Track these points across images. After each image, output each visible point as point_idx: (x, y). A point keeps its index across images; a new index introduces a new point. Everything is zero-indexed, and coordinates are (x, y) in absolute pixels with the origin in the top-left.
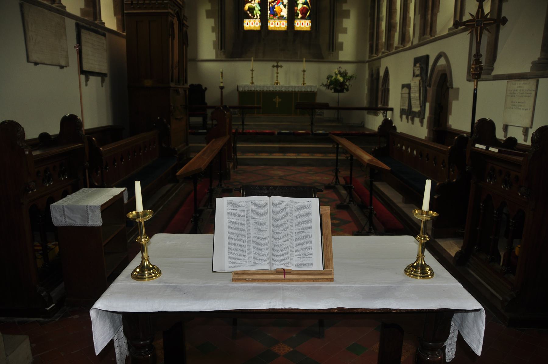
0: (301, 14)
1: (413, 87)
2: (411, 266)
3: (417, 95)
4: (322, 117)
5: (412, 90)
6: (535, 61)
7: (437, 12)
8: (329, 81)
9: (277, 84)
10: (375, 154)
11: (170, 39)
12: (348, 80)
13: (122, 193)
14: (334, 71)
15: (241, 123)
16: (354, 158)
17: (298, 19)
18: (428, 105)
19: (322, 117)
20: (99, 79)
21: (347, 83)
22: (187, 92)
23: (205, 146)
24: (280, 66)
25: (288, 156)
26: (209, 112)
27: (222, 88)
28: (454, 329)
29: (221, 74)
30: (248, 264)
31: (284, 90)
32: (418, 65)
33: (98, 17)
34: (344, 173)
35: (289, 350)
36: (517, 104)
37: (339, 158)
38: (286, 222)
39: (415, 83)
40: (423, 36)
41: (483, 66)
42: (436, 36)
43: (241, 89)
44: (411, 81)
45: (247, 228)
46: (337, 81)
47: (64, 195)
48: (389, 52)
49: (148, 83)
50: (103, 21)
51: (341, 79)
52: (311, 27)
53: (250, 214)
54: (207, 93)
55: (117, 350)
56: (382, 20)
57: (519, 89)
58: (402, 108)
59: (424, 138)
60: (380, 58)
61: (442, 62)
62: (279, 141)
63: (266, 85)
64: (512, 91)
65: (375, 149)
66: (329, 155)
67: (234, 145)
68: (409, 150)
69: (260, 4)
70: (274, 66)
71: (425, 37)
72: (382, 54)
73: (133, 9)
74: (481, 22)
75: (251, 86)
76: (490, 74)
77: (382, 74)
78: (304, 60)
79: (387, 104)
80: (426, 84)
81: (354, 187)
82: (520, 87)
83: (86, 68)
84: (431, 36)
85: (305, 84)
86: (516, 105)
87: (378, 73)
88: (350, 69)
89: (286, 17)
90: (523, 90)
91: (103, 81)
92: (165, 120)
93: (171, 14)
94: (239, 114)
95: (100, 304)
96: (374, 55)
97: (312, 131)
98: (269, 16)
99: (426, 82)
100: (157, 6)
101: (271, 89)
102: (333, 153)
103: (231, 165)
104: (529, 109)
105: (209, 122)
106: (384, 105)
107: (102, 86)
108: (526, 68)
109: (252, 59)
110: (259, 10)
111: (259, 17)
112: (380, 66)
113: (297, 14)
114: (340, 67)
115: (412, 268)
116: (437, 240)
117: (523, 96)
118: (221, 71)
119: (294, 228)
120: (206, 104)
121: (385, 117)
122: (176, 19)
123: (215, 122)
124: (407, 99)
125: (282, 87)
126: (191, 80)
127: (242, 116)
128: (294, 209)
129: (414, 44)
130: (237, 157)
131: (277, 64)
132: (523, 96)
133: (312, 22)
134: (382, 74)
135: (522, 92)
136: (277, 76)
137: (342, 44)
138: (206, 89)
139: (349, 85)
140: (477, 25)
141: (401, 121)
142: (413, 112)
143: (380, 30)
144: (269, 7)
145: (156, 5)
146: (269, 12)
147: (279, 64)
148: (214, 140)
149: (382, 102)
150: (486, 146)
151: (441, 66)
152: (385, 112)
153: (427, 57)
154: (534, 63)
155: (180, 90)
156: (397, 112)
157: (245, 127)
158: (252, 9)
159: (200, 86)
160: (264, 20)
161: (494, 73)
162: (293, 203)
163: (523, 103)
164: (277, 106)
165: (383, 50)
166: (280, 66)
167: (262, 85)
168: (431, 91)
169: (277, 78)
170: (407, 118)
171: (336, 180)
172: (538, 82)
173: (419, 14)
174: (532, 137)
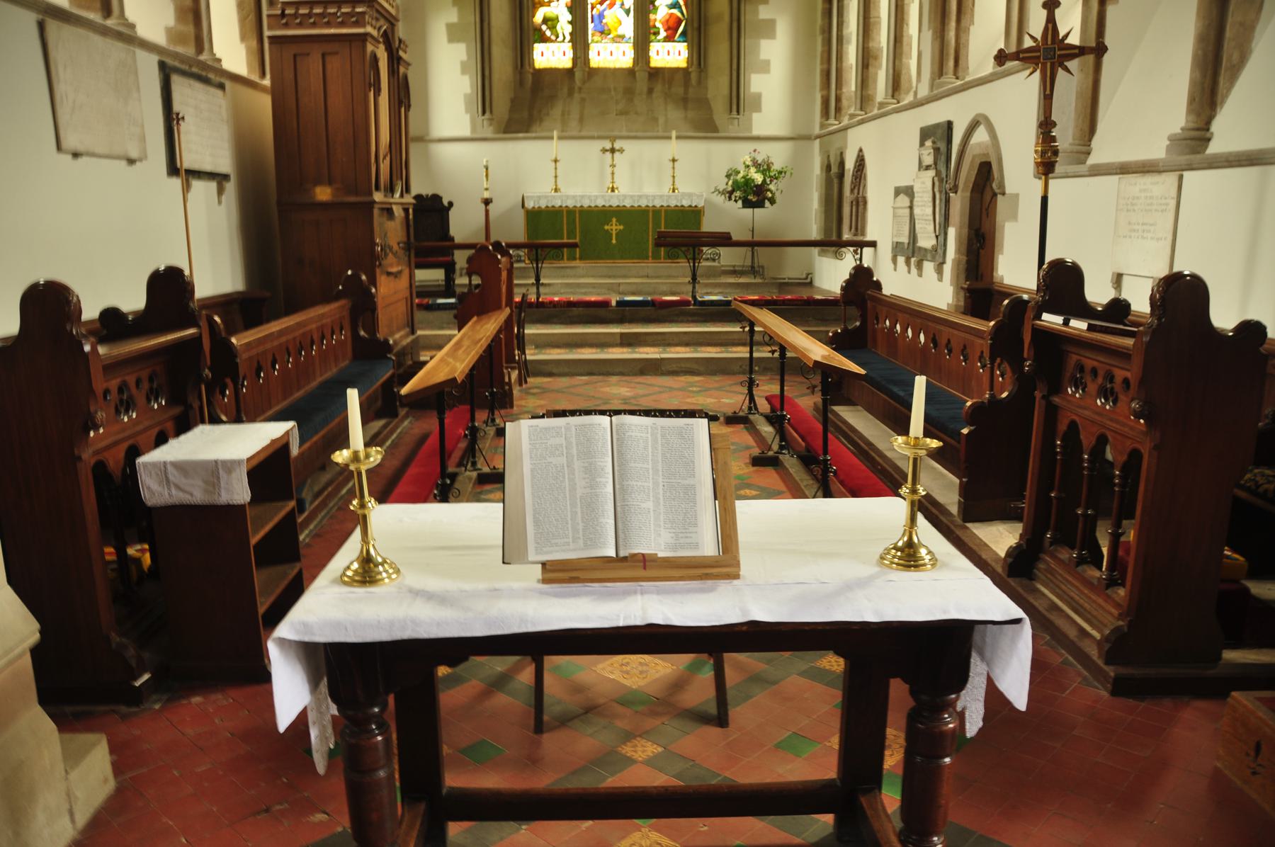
0: (666, 31)
1: (917, 192)
2: (892, 548)
3: (929, 210)
4: (716, 264)
5: (915, 199)
6: (1176, 135)
7: (970, 25)
8: (730, 183)
9: (613, 190)
10: (837, 343)
11: (372, 94)
12: (773, 178)
13: (287, 433)
14: (742, 160)
15: (533, 281)
16: (789, 354)
17: (659, 41)
18: (952, 232)
19: (716, 264)
20: (213, 185)
21: (772, 187)
22: (411, 211)
23: (455, 335)
24: (618, 150)
25: (640, 353)
26: (461, 258)
27: (487, 202)
28: (978, 670)
29: (485, 170)
30: (572, 546)
31: (628, 206)
32: (929, 143)
33: (206, 46)
34: (767, 387)
35: (655, 751)
37: (756, 355)
38: (645, 466)
39: (923, 183)
40: (939, 79)
41: (1059, 148)
42: (968, 79)
43: (530, 205)
44: (914, 180)
45: (569, 478)
46: (748, 182)
47: (161, 440)
48: (866, 114)
49: (323, 194)
50: (218, 56)
51: (758, 178)
52: (690, 60)
53: (574, 451)
54: (453, 214)
55: (314, 733)
56: (849, 42)
58: (896, 240)
59: (945, 308)
60: (846, 129)
61: (981, 136)
62: (621, 321)
63: (588, 194)
65: (835, 333)
66: (734, 349)
67: (518, 330)
68: (898, 327)
69: (571, 9)
70: (604, 151)
71: (942, 80)
72: (850, 119)
73: (286, 26)
74: (1052, 53)
75: (554, 197)
76: (1084, 162)
77: (850, 165)
78: (674, 134)
79: (863, 234)
80: (947, 186)
81: (789, 416)
82: (1145, 190)
83: (188, 159)
84: (957, 78)
85: (677, 189)
86: (1138, 230)
87: (842, 164)
88: (778, 155)
89: (630, 38)
90: (1151, 197)
91: (220, 191)
92: (364, 277)
93: (372, 37)
94: (527, 262)
95: (286, 629)
96: (832, 121)
97: (694, 297)
98: (593, 35)
99: (947, 181)
100: (340, 20)
101: (600, 203)
102: (744, 345)
103: (514, 375)
104: (1165, 239)
105: (461, 281)
106: (855, 235)
107: (220, 202)
108: (1157, 150)
109: (555, 134)
110: (570, 22)
111: (568, 37)
112: (846, 147)
113: (656, 30)
114: (755, 151)
115: (894, 551)
116: (969, 525)
117: (1151, 210)
118: (485, 163)
119: (661, 477)
120: (452, 239)
121: (858, 262)
122: (382, 47)
123: (476, 280)
125: (625, 196)
126: (420, 186)
127: (535, 265)
128: (659, 439)
129: (919, 96)
130: (526, 357)
131: (613, 145)
132: (1151, 210)
133: (690, 48)
134: (850, 165)
136: (613, 174)
137: (758, 97)
138: (451, 204)
139: (777, 190)
140: (1044, 59)
142: (920, 248)
143: (844, 64)
144: (592, 15)
145: (338, 17)
146: (591, 26)
147: (617, 145)
148: (475, 318)
149: (850, 230)
150: (1063, 318)
151: (979, 144)
152: (859, 251)
153: (949, 125)
154: (1173, 139)
155: (394, 207)
156: (885, 249)
157: (542, 290)
158: (550, 21)
159: (436, 198)
160: (580, 41)
161: (1092, 160)
162: (656, 428)
163: (1151, 225)
164: (614, 241)
165: (852, 111)
166: (618, 150)
167: (578, 194)
168: (959, 203)
169: (613, 179)
170: (908, 263)
171: (750, 403)
172: (1181, 178)
173: (929, 29)
174: (1151, 295)
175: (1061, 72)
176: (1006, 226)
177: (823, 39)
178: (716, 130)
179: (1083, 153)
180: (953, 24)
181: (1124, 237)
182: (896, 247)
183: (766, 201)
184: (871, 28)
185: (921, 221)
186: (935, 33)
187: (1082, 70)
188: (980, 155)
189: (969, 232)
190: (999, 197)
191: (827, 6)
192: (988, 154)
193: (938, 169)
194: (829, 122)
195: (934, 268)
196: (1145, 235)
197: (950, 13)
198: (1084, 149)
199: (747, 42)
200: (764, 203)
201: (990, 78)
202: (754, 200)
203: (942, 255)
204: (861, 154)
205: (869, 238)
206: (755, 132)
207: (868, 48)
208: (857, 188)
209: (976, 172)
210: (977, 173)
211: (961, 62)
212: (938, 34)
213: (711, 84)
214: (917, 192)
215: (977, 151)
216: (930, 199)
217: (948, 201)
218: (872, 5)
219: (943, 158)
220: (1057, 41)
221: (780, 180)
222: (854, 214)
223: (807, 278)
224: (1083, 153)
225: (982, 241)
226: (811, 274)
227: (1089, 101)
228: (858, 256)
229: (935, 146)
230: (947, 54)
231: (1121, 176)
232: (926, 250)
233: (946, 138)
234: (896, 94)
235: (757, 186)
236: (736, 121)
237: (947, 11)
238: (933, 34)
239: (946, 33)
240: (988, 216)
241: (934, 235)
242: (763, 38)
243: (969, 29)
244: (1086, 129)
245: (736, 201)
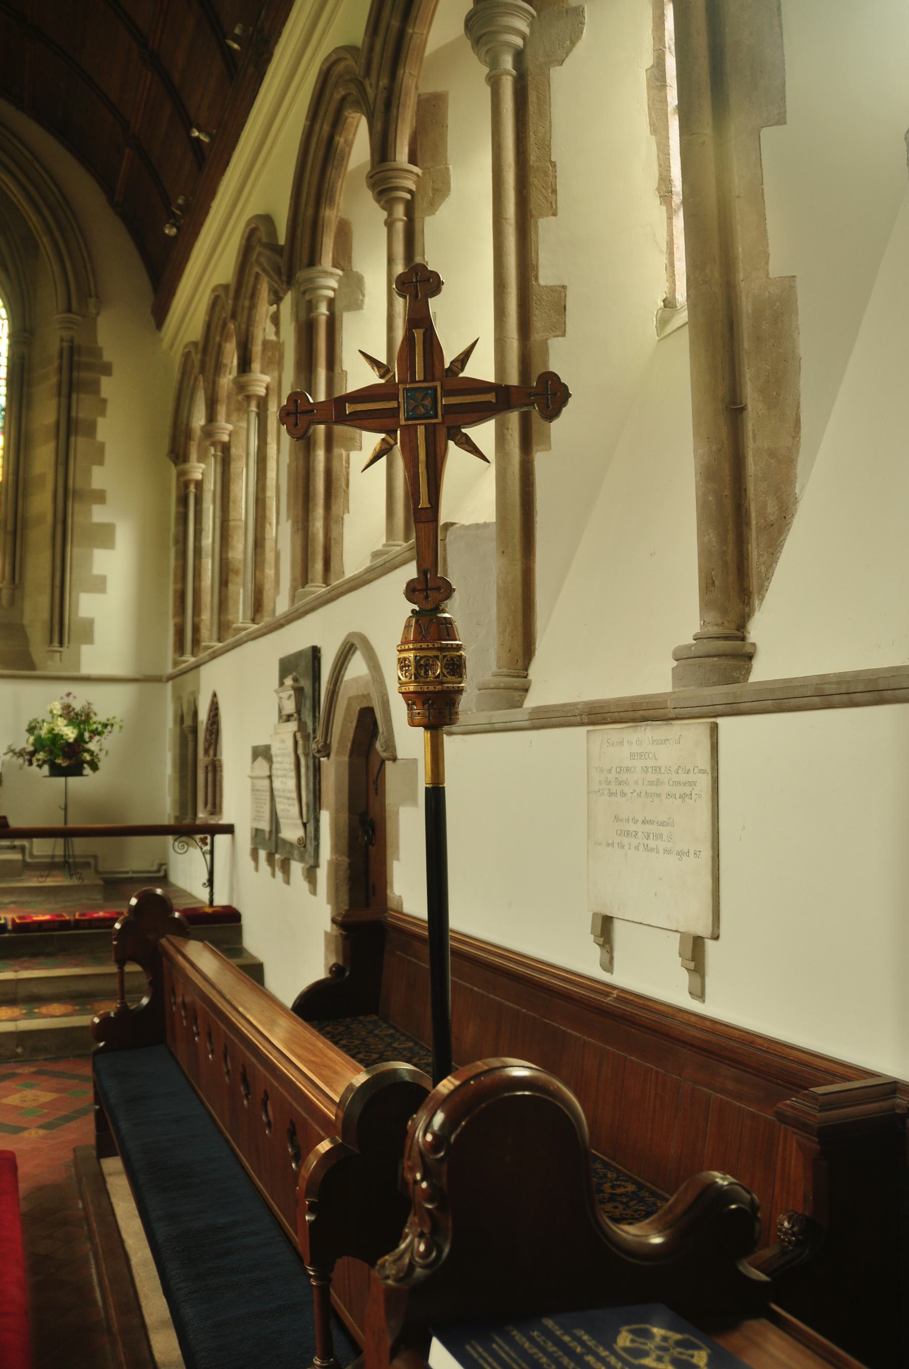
1: (276, 756)
3: (292, 783)
7: (343, 514)
8: (32, 739)
12: (95, 733)
21: (92, 746)
36: (640, 827)
39: (283, 741)
40: (303, 587)
46: (55, 738)
51: (70, 734)
57: (639, 763)
60: (197, 666)
61: (357, 668)
64: (610, 771)
71: (308, 588)
74: (428, 402)
77: (203, 716)
82: (641, 755)
87: (195, 714)
90: (657, 769)
114: (69, 694)
124: (267, 796)
134: (203, 716)
135: (652, 777)
139: (100, 750)
140: (407, 419)
141: (257, 869)
142: (285, 842)
151: (355, 680)
152: (209, 841)
153: (315, 652)
154: (681, 656)
161: (532, 701)
163: (662, 824)
170: (270, 859)
172: (714, 728)
173: (287, 520)
175: (455, 453)
176: (400, 813)
177: (177, 552)
178: (32, 666)
179: (516, 689)
180: (319, 511)
181: (608, 845)
182: (256, 836)
183: (85, 766)
184: (230, 533)
185: (282, 799)
186: (295, 523)
187: (503, 552)
188: (357, 697)
189: (350, 818)
190: (388, 764)
191: (182, 510)
192: (369, 694)
193: (303, 720)
194: (184, 658)
195: (303, 875)
196: (652, 843)
197: (315, 495)
198: (517, 682)
199: (75, 552)
200: (82, 768)
201: (366, 577)
202: (64, 765)
203: (312, 853)
204: (215, 700)
205: (225, 820)
206: (85, 671)
207: (227, 559)
208: (212, 747)
209: (354, 724)
210: (357, 727)
211: (334, 565)
212: (300, 526)
213: (28, 606)
214: (276, 756)
215: (353, 692)
216: (292, 766)
217: (317, 769)
218: (231, 504)
219: (308, 703)
220: (438, 374)
221: (104, 736)
222: (210, 784)
223: (158, 871)
224: (516, 689)
225: (370, 832)
226: (165, 864)
227: (520, 604)
228: (208, 848)
229: (297, 685)
230: (314, 553)
231: (591, 728)
232: (291, 844)
233: (311, 674)
234: (258, 616)
235: (68, 744)
236: (58, 654)
237: (311, 493)
238: (293, 526)
239: (310, 524)
240: (377, 794)
241: (300, 822)
242: (98, 547)
243: (342, 519)
244: (519, 650)
245: (40, 766)
